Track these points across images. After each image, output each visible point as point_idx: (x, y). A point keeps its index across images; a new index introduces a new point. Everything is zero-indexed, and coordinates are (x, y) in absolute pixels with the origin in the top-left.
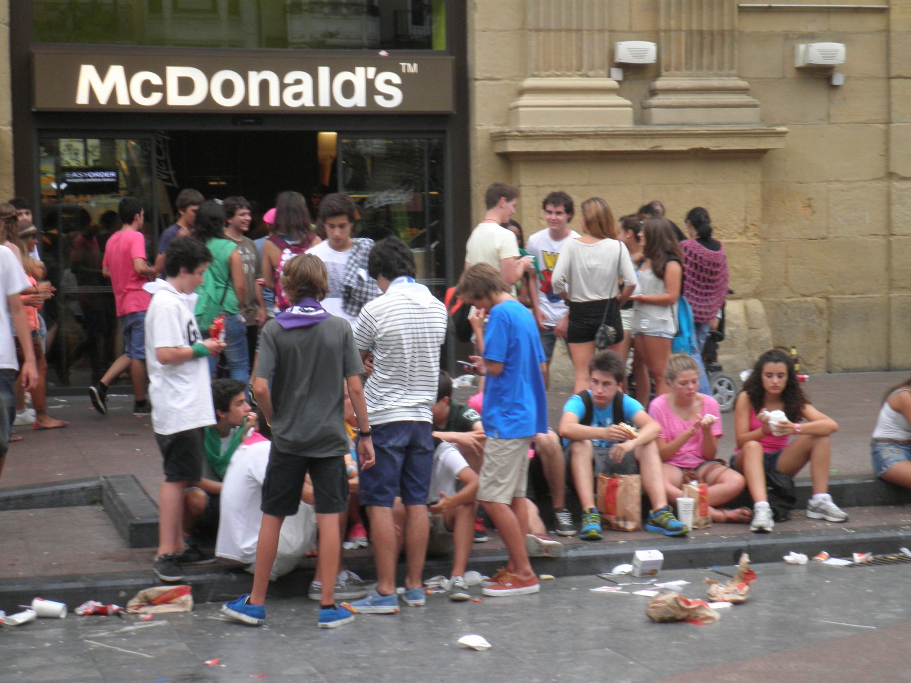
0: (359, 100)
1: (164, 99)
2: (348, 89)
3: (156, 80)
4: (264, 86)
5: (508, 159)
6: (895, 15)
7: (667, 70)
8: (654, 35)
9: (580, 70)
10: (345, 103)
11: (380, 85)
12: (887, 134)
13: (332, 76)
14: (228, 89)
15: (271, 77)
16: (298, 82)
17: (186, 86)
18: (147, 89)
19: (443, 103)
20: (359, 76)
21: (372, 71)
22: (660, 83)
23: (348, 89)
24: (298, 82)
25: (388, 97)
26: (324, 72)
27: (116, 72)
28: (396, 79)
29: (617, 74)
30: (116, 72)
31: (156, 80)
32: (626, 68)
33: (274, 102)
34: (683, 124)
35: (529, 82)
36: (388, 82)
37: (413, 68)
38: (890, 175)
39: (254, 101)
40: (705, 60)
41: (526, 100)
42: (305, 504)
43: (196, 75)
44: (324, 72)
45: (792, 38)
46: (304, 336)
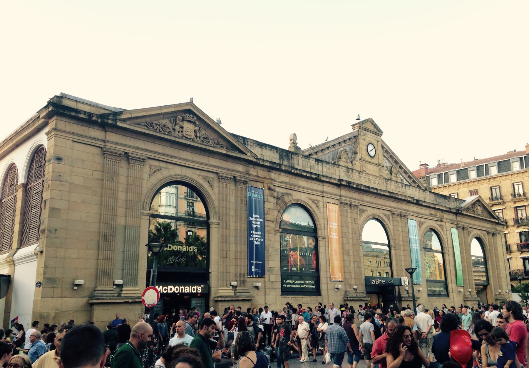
0: (195, 291)
1: (168, 291)
2: (194, 289)
3: (167, 288)
4: (182, 289)
5: (217, 301)
8: (236, 281)
10: (193, 292)
11: (198, 289)
12: (265, 297)
13: (179, 291)
16: (187, 288)
17: (171, 289)
18: (165, 290)
19: (207, 292)
20: (195, 287)
21: (197, 286)
23: (194, 289)
24: (187, 288)
25: (199, 291)
26: (191, 287)
27: (161, 287)
29: (231, 287)
30: (161, 287)
31: (167, 288)
32: (232, 286)
33: (183, 292)
35: (220, 288)
37: (203, 286)
41: (220, 291)
43: (172, 287)
44: (191, 287)
46: (523, 250)
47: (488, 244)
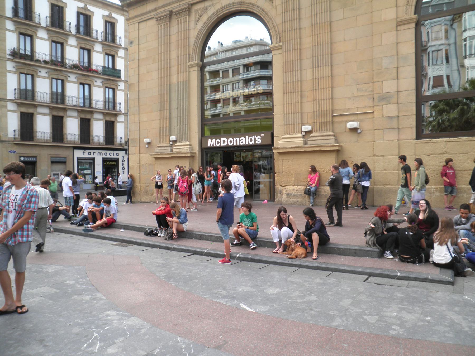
3: (219, 141)
4: (237, 141)
6: (375, 113)
7: (314, 131)
9: (295, 133)
10: (251, 143)
11: (257, 139)
14: (231, 142)
15: (238, 139)
16: (242, 139)
17: (224, 142)
18: (218, 143)
20: (253, 138)
22: (177, 144)
23: (251, 140)
24: (242, 139)
25: (258, 141)
28: (260, 137)
31: (219, 141)
33: (238, 144)
34: (315, 144)
36: (258, 138)
37: (263, 135)
38: (375, 155)
39: (235, 144)
40: (323, 129)
42: (12, 162)
43: (225, 139)
44: (247, 137)
45: (347, 122)
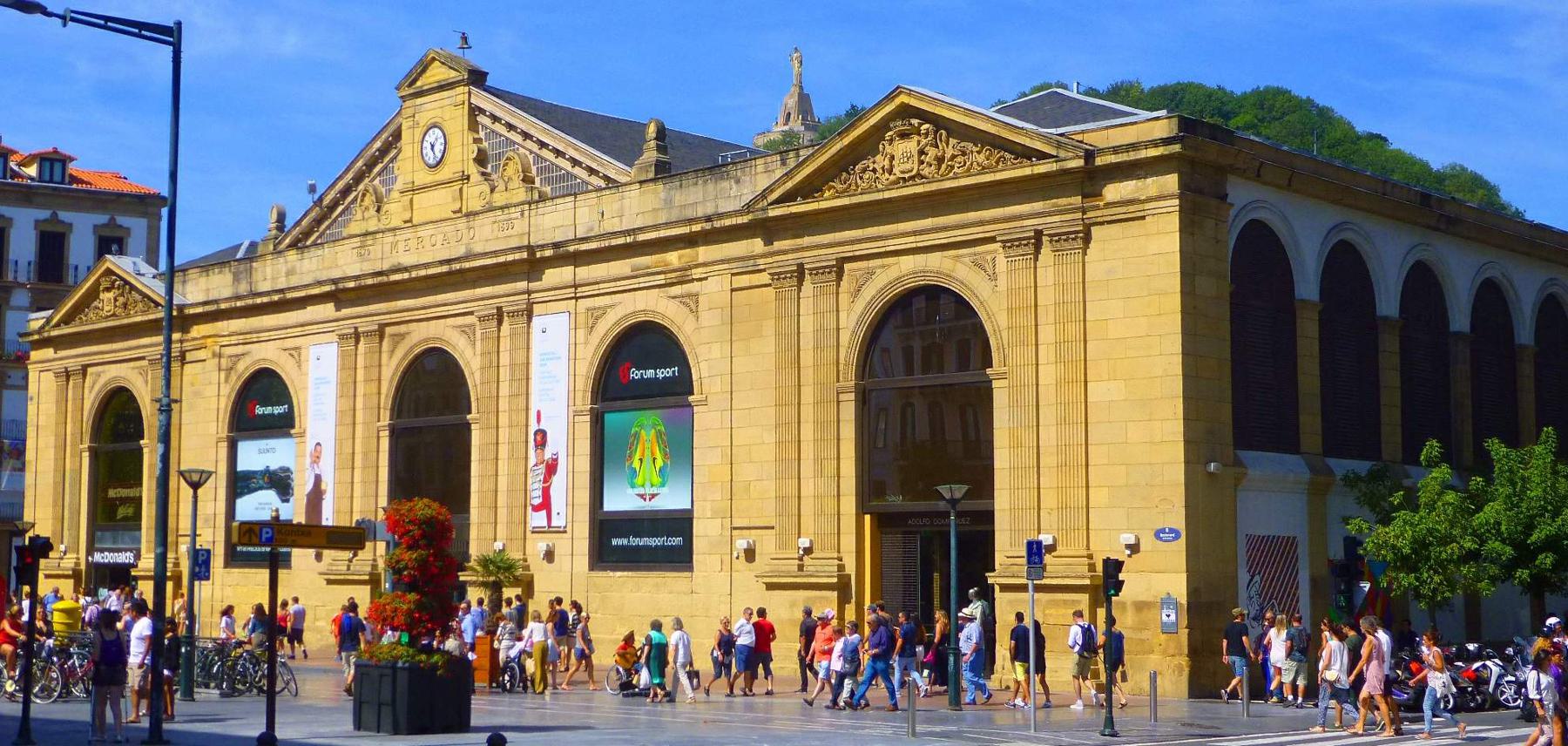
47: (1002, 319)
